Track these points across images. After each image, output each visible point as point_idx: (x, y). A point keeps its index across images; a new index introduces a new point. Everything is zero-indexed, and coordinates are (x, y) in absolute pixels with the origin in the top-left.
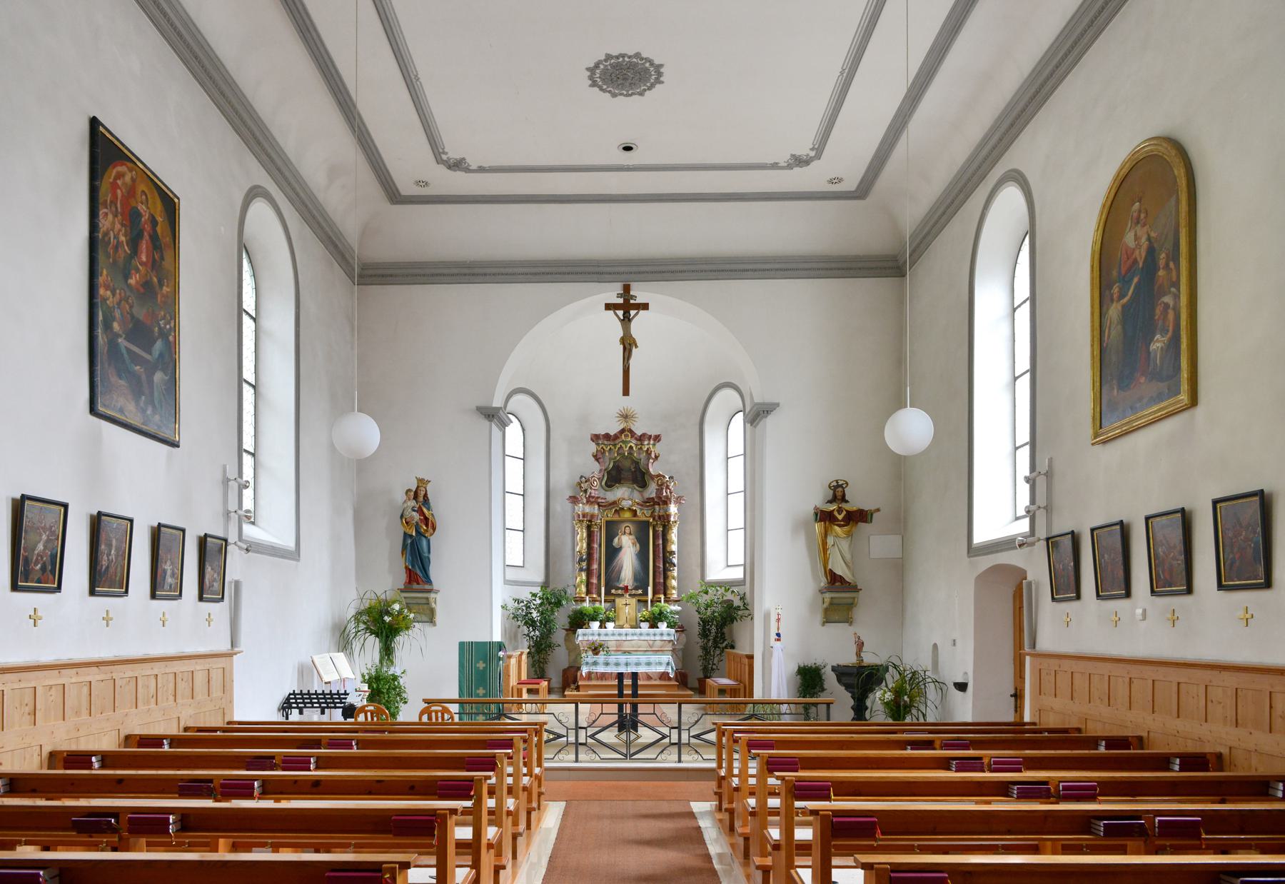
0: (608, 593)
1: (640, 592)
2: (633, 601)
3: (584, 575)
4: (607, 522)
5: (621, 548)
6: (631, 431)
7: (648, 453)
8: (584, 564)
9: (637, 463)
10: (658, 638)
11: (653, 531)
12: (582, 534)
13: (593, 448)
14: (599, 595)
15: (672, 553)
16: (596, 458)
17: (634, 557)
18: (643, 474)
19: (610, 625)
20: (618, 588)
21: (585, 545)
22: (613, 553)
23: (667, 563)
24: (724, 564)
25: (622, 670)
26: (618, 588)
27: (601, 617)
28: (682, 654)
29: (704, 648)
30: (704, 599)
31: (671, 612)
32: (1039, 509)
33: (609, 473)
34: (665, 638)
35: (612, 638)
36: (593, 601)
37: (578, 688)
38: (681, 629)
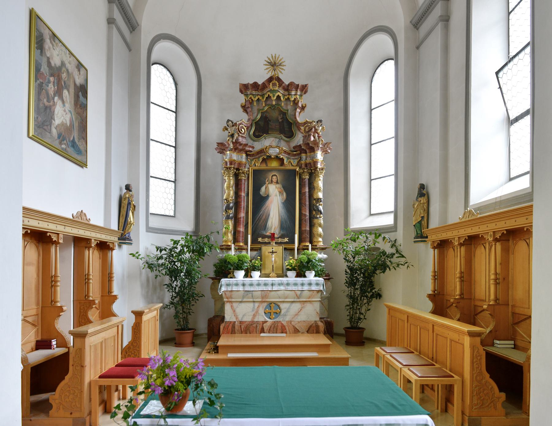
0: (254, 241)
1: (286, 240)
2: (280, 249)
3: (231, 223)
4: (255, 171)
5: (268, 197)
6: (279, 79)
7: (296, 103)
8: (231, 212)
9: (284, 114)
10: (306, 288)
11: (300, 179)
12: (230, 181)
13: (242, 99)
14: (246, 244)
15: (319, 200)
16: (245, 108)
17: (281, 205)
18: (290, 124)
19: (256, 274)
21: (232, 193)
22: (260, 201)
23: (314, 210)
24: (366, 213)
26: (264, 237)
28: (328, 302)
29: (353, 299)
30: (352, 247)
31: (320, 260)
32: (417, 197)
34: (314, 288)
35: (257, 288)
36: (240, 249)
37: (216, 349)
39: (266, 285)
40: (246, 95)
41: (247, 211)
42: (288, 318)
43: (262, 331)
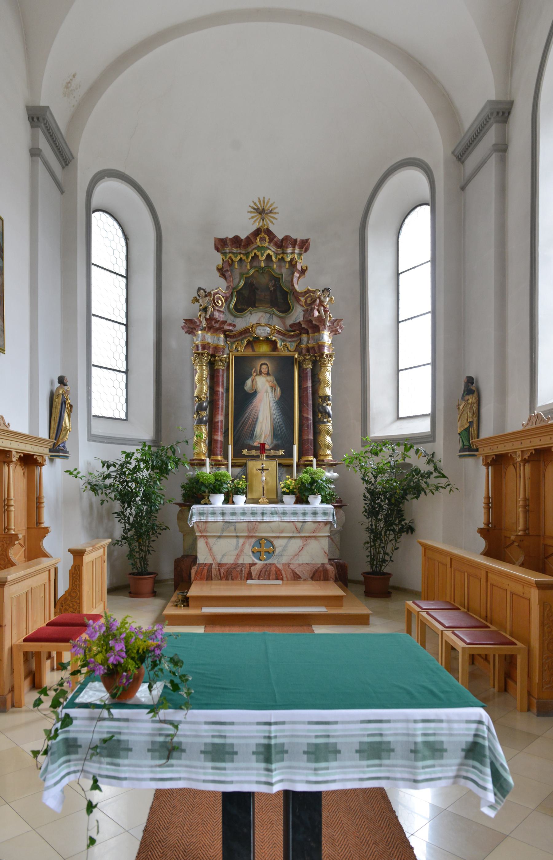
0: (237, 454)
1: (281, 452)
2: (273, 465)
3: (204, 430)
4: (238, 359)
5: (255, 393)
6: (269, 232)
7: (293, 264)
8: (205, 414)
9: (277, 280)
10: (309, 518)
11: (299, 369)
12: (202, 372)
13: (218, 259)
14: (226, 457)
15: (326, 398)
16: (222, 272)
17: (273, 405)
18: (285, 294)
19: (240, 500)
20: (251, 448)
22: (244, 399)
23: (319, 413)
24: (392, 417)
25: (243, 778)
26: (251, 448)
27: (226, 487)
28: (340, 537)
29: (375, 534)
30: (372, 462)
31: (329, 481)
32: (461, 394)
33: (239, 293)
34: (320, 518)
35: (242, 519)
36: (217, 465)
38: (340, 505)
39: (253, 514)
40: (224, 254)
41: (226, 414)
42: (285, 560)
43: (249, 576)
